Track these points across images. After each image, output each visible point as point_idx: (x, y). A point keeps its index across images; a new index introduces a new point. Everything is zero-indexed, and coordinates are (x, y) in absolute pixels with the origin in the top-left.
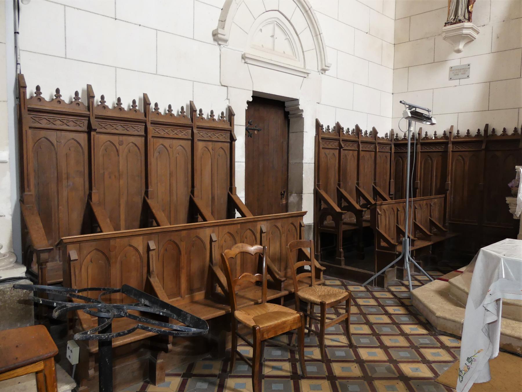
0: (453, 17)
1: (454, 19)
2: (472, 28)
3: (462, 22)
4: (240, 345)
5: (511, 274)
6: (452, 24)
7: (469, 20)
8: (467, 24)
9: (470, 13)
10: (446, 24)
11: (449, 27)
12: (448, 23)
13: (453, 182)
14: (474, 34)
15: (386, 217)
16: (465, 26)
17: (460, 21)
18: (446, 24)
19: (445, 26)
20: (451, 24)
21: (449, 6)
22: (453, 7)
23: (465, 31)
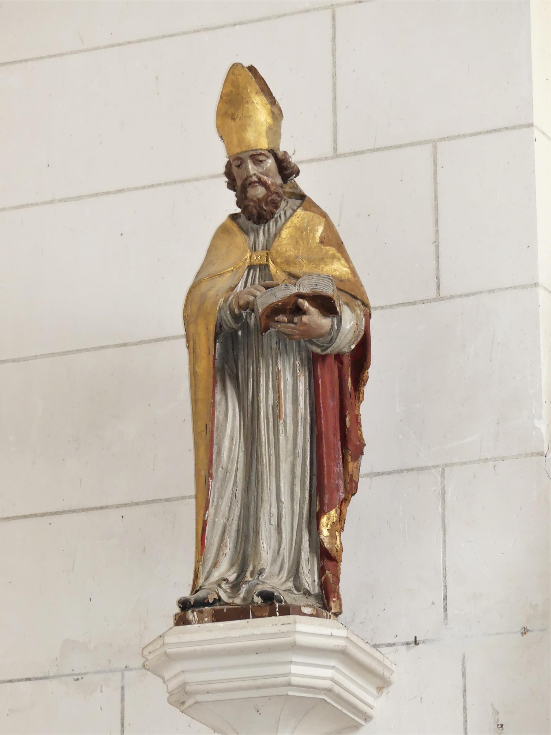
0: (225, 570)
1: (236, 587)
2: (343, 654)
3: (286, 611)
4: (190, 497)
5: (325, 468)
6: (224, 614)
7: (327, 598)
8: (309, 628)
9: (328, 559)
10: (184, 605)
11: (207, 633)
12: (201, 603)
13: (295, 533)
14: (359, 690)
15: (257, 451)
16: (301, 640)
17: (270, 604)
18: (184, 605)
19: (181, 620)
20: (219, 617)
21: (203, 502)
22: (225, 509)
23: (306, 672)
